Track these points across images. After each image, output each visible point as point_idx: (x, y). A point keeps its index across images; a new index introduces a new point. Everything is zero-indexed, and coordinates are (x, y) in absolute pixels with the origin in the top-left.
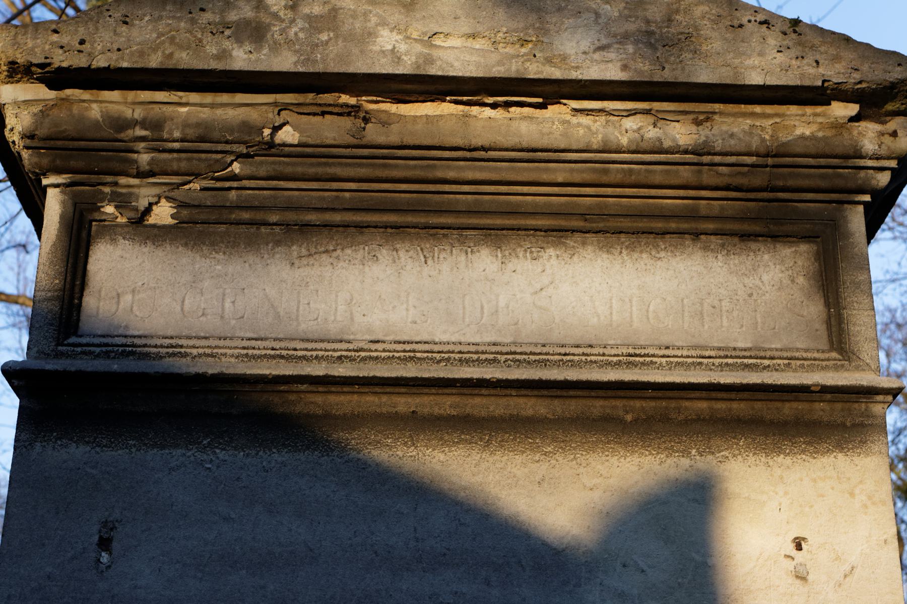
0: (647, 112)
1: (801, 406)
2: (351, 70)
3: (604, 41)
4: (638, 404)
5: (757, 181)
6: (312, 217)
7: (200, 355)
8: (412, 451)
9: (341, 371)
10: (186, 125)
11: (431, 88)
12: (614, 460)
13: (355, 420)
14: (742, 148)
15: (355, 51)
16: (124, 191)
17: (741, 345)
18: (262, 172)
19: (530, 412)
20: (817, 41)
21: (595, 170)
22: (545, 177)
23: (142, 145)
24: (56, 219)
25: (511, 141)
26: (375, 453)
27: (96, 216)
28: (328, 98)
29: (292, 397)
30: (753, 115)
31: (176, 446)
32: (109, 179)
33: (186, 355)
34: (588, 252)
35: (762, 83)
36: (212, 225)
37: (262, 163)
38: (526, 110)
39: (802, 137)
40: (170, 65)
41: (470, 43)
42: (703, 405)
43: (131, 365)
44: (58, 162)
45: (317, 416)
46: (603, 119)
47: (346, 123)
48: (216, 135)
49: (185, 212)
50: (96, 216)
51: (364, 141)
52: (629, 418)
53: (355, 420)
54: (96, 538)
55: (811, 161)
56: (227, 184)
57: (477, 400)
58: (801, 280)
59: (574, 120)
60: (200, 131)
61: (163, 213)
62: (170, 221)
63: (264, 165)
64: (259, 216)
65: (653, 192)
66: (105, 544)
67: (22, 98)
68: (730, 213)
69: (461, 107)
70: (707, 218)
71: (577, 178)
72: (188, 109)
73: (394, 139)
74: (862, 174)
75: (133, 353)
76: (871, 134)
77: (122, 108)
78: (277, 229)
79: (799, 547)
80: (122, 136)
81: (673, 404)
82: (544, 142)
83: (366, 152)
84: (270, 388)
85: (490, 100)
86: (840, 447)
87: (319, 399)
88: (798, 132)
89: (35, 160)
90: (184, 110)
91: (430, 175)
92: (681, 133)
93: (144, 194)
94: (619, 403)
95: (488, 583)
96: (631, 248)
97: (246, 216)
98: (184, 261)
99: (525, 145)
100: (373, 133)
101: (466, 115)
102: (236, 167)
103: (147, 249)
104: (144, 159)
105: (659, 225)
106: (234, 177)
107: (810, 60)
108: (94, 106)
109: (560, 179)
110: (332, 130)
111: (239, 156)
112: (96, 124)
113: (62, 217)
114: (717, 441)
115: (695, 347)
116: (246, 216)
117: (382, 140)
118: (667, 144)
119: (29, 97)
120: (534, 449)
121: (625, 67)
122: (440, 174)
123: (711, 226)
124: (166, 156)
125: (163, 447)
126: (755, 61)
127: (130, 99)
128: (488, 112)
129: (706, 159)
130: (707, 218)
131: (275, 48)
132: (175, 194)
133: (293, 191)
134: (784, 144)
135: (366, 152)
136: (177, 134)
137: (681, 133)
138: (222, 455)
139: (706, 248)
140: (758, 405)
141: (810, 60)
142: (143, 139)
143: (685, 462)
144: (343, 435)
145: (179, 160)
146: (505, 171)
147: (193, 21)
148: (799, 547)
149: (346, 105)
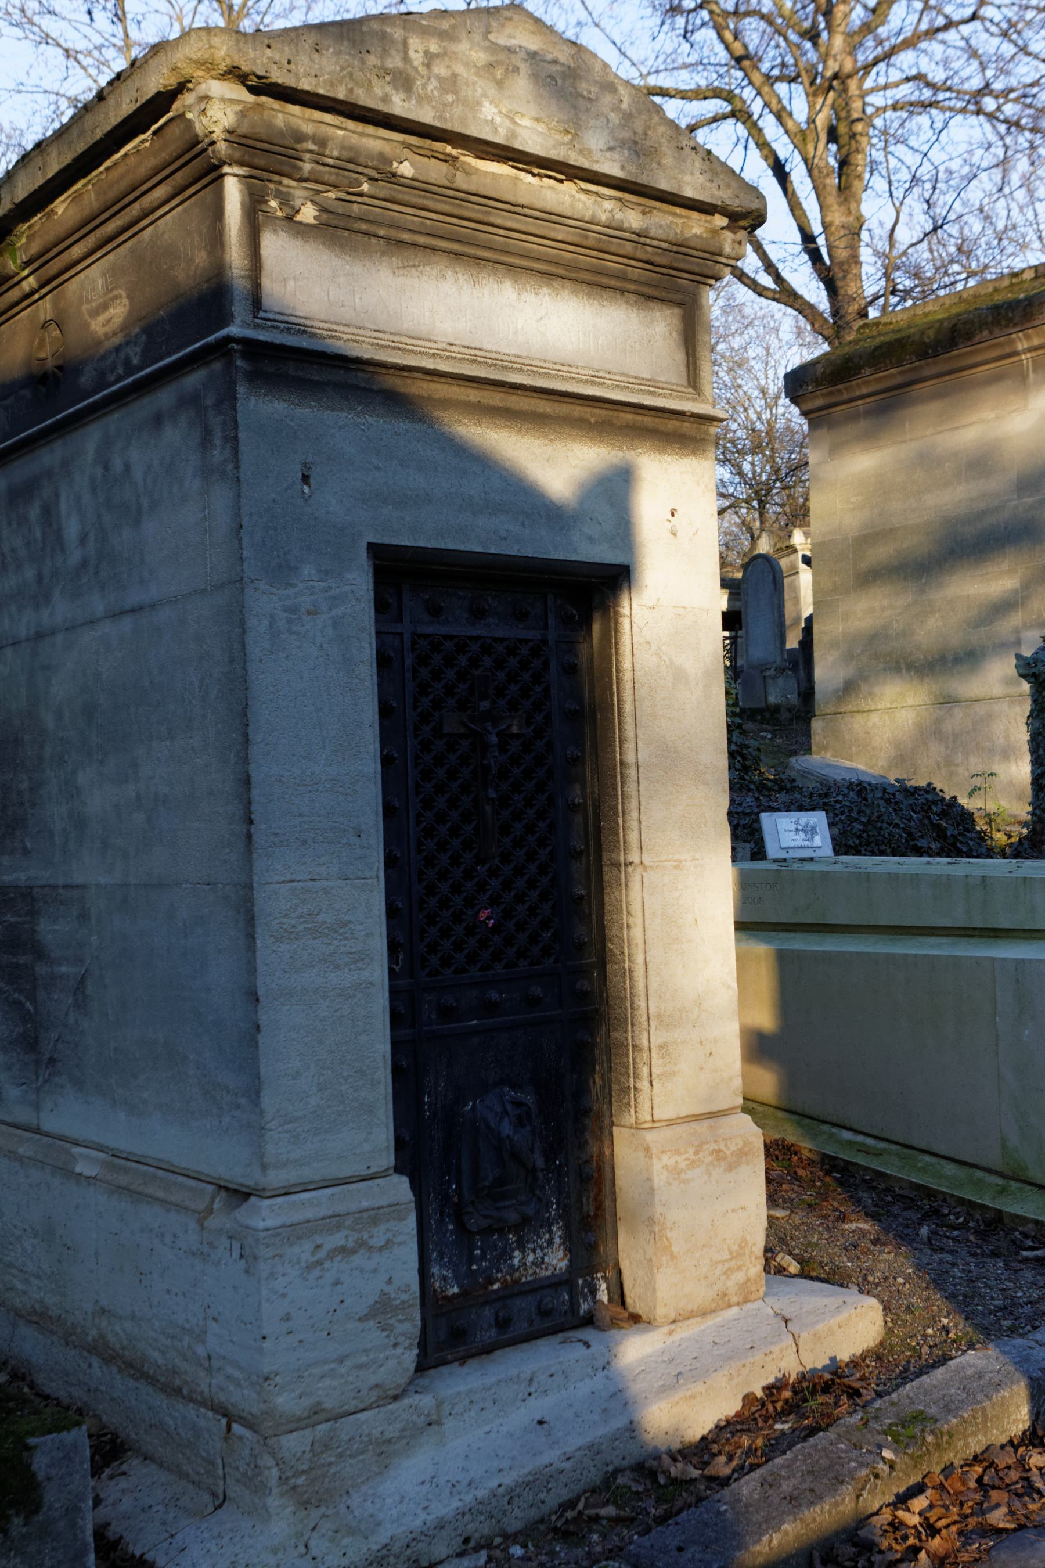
0: (620, 199)
1: (677, 423)
2: (468, 133)
3: (612, 144)
4: (598, 411)
5: (664, 261)
6: (406, 236)
7: (349, 340)
8: (479, 430)
9: (443, 367)
10: (343, 147)
11: (503, 153)
12: (585, 448)
13: (446, 404)
14: (663, 237)
15: (470, 116)
16: (284, 189)
17: (645, 376)
18: (382, 194)
19: (541, 410)
20: (719, 169)
21: (581, 235)
22: (552, 235)
23: (307, 156)
24: (238, 206)
25: (540, 205)
26: (459, 429)
27: (264, 207)
28: (438, 146)
29: (409, 381)
30: (675, 214)
31: (342, 410)
32: (276, 178)
33: (340, 339)
34: (565, 294)
35: (362, 14)
36: (339, 230)
37: (383, 187)
38: (552, 182)
39: (695, 235)
40: (352, 99)
41: (535, 125)
42: (630, 417)
43: (305, 343)
44: (246, 158)
45: (423, 397)
46: (593, 198)
47: (444, 167)
48: (362, 160)
49: (325, 216)
50: (264, 207)
51: (454, 186)
52: (593, 420)
53: (446, 404)
54: (300, 475)
55: (695, 253)
56: (354, 198)
57: (514, 398)
58: (674, 334)
59: (578, 196)
60: (352, 154)
61: (308, 214)
62: (312, 221)
63: (384, 189)
64: (373, 229)
65: (606, 256)
66: (305, 479)
67: (228, 96)
68: (643, 279)
69: (515, 171)
70: (631, 281)
71: (569, 239)
72: (343, 133)
73: (473, 188)
74: (718, 266)
75: (304, 332)
76: (729, 241)
77: (299, 122)
78: (382, 241)
79: (673, 515)
80: (298, 146)
81: (616, 414)
82: (559, 209)
83: (451, 193)
84: (398, 373)
85: (536, 171)
86: (694, 453)
87: (425, 385)
88: (694, 231)
89: (230, 152)
90: (340, 133)
91: (485, 219)
92: (633, 219)
93: (298, 193)
94: (588, 410)
95: (523, 525)
96: (589, 295)
97: (364, 227)
98: (325, 257)
99: (548, 209)
100: (461, 181)
101: (517, 178)
102: (365, 187)
103: (299, 243)
104: (307, 167)
105: (605, 281)
106: (361, 195)
107: (715, 184)
108: (280, 115)
109: (560, 238)
110: (436, 171)
111: (372, 179)
112: (281, 133)
113: (242, 204)
114: (636, 442)
115: (623, 374)
116: (364, 227)
117: (465, 187)
118: (626, 225)
119: (234, 96)
120: (546, 436)
121: (623, 168)
122: (492, 220)
123: (632, 287)
124: (321, 168)
125: (333, 410)
126: (687, 178)
127: (307, 116)
128: (529, 178)
129: (642, 240)
130: (631, 281)
131: (420, 100)
132: (317, 198)
133: (410, 217)
134: (686, 239)
135: (451, 193)
136: (335, 154)
137: (633, 219)
138: (370, 419)
139: (627, 303)
140: (657, 420)
141: (715, 184)
142: (311, 152)
143: (621, 454)
144: (438, 413)
145: (330, 173)
146: (530, 225)
147: (363, 61)
148: (673, 515)
149: (449, 155)
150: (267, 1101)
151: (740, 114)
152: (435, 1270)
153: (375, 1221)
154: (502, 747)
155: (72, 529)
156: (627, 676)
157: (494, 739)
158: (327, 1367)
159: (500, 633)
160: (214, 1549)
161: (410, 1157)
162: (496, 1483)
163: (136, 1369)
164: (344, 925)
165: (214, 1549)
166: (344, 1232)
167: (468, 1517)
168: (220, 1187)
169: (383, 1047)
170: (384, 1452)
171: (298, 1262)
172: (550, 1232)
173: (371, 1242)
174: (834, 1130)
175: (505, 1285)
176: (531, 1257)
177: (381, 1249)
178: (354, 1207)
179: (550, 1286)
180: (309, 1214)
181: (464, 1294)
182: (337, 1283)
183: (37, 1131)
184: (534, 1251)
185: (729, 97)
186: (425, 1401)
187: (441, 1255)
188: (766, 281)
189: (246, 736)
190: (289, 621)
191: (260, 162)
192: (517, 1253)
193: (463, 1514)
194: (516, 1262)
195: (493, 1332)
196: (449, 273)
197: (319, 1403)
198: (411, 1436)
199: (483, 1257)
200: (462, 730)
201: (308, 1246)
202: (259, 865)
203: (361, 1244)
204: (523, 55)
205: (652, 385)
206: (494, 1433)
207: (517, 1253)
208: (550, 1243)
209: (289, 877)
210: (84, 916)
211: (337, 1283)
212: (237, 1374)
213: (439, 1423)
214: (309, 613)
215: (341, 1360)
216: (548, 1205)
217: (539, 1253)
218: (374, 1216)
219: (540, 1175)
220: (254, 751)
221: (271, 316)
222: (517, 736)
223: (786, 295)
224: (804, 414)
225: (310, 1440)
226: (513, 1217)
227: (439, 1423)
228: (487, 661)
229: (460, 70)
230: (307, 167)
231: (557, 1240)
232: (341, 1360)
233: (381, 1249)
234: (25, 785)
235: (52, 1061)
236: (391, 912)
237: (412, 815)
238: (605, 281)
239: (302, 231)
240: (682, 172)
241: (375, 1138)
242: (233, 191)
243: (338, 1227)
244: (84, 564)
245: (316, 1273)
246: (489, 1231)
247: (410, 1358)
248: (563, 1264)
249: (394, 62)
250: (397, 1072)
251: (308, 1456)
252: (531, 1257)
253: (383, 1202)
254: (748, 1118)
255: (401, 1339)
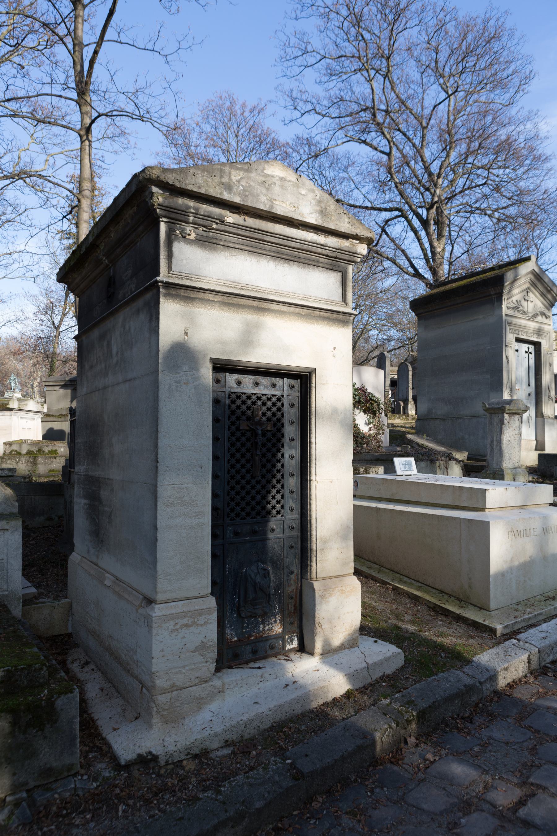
22: (289, 245)
23: (191, 215)
96: (304, 267)
111: (217, 223)
121: (316, 220)
150: (159, 567)
151: (403, 215)
152: (228, 631)
153: (200, 614)
154: (264, 435)
155: (114, 350)
156: (313, 410)
157: (260, 432)
158: (177, 670)
159: (264, 392)
160: (130, 737)
161: (218, 587)
162: (240, 719)
163: (117, 659)
164: (193, 501)
165: (130, 737)
166: (187, 619)
167: (228, 733)
168: (145, 597)
169: (208, 547)
170: (200, 703)
171: (168, 629)
172: (275, 618)
173: (198, 622)
174: (402, 577)
175: (256, 638)
176: (267, 627)
177: (202, 625)
178: (192, 609)
179: (274, 638)
180: (173, 611)
181: (239, 640)
182: (184, 637)
183: (97, 565)
184: (268, 625)
185: (399, 210)
186: (217, 683)
187: (231, 626)
188: (410, 270)
189: (157, 429)
190: (177, 386)
191: (173, 215)
192: (261, 626)
193: (226, 731)
194: (261, 629)
195: (251, 655)
196: (248, 258)
197: (174, 683)
198: (211, 697)
199: (248, 627)
200: (248, 428)
201: (172, 623)
202: (160, 478)
203: (194, 623)
204: (278, 178)
205: (329, 301)
206: (239, 701)
207: (261, 626)
208: (275, 622)
209: (172, 483)
210: (112, 490)
211: (184, 637)
212: (145, 669)
213: (223, 692)
214: (185, 383)
215: (184, 667)
216: (275, 607)
217: (271, 626)
218: (200, 613)
219: (272, 596)
220: (160, 435)
221: (175, 273)
222: (270, 431)
223: (417, 275)
224: (416, 315)
225: (169, 698)
226: (260, 612)
227: (223, 692)
228: (259, 403)
229: (252, 184)
230: (191, 219)
231: (278, 621)
232: (184, 667)
233: (202, 625)
234: (99, 441)
235: (102, 541)
236: (215, 495)
237: (226, 460)
238: (310, 263)
239: (191, 242)
240: (340, 222)
241: (205, 583)
242: (163, 227)
243: (185, 617)
244: (117, 363)
245: (175, 634)
246: (251, 617)
247: (213, 666)
248: (280, 630)
249: (225, 180)
250: (214, 556)
251: (168, 703)
252: (267, 627)
253: (205, 607)
254: (355, 577)
255: (209, 659)
